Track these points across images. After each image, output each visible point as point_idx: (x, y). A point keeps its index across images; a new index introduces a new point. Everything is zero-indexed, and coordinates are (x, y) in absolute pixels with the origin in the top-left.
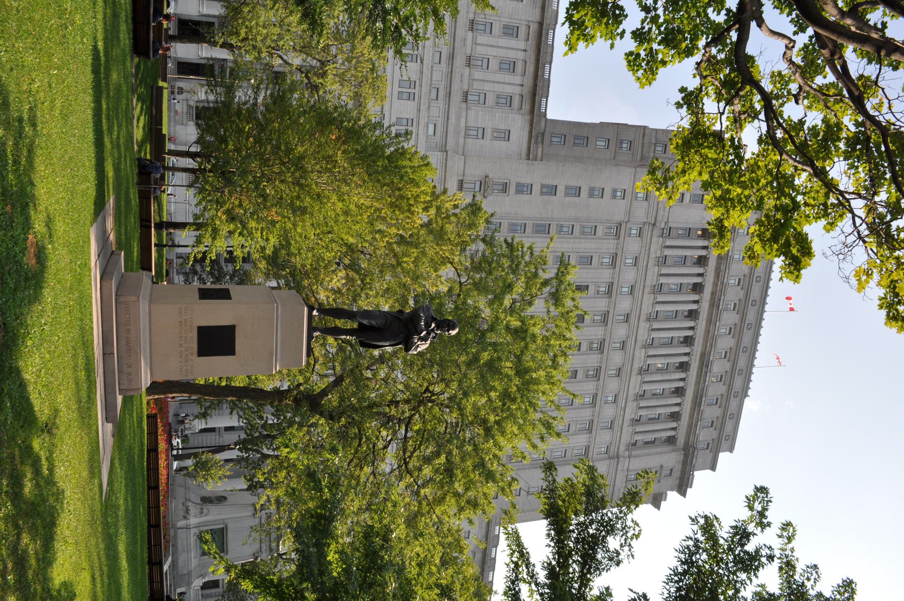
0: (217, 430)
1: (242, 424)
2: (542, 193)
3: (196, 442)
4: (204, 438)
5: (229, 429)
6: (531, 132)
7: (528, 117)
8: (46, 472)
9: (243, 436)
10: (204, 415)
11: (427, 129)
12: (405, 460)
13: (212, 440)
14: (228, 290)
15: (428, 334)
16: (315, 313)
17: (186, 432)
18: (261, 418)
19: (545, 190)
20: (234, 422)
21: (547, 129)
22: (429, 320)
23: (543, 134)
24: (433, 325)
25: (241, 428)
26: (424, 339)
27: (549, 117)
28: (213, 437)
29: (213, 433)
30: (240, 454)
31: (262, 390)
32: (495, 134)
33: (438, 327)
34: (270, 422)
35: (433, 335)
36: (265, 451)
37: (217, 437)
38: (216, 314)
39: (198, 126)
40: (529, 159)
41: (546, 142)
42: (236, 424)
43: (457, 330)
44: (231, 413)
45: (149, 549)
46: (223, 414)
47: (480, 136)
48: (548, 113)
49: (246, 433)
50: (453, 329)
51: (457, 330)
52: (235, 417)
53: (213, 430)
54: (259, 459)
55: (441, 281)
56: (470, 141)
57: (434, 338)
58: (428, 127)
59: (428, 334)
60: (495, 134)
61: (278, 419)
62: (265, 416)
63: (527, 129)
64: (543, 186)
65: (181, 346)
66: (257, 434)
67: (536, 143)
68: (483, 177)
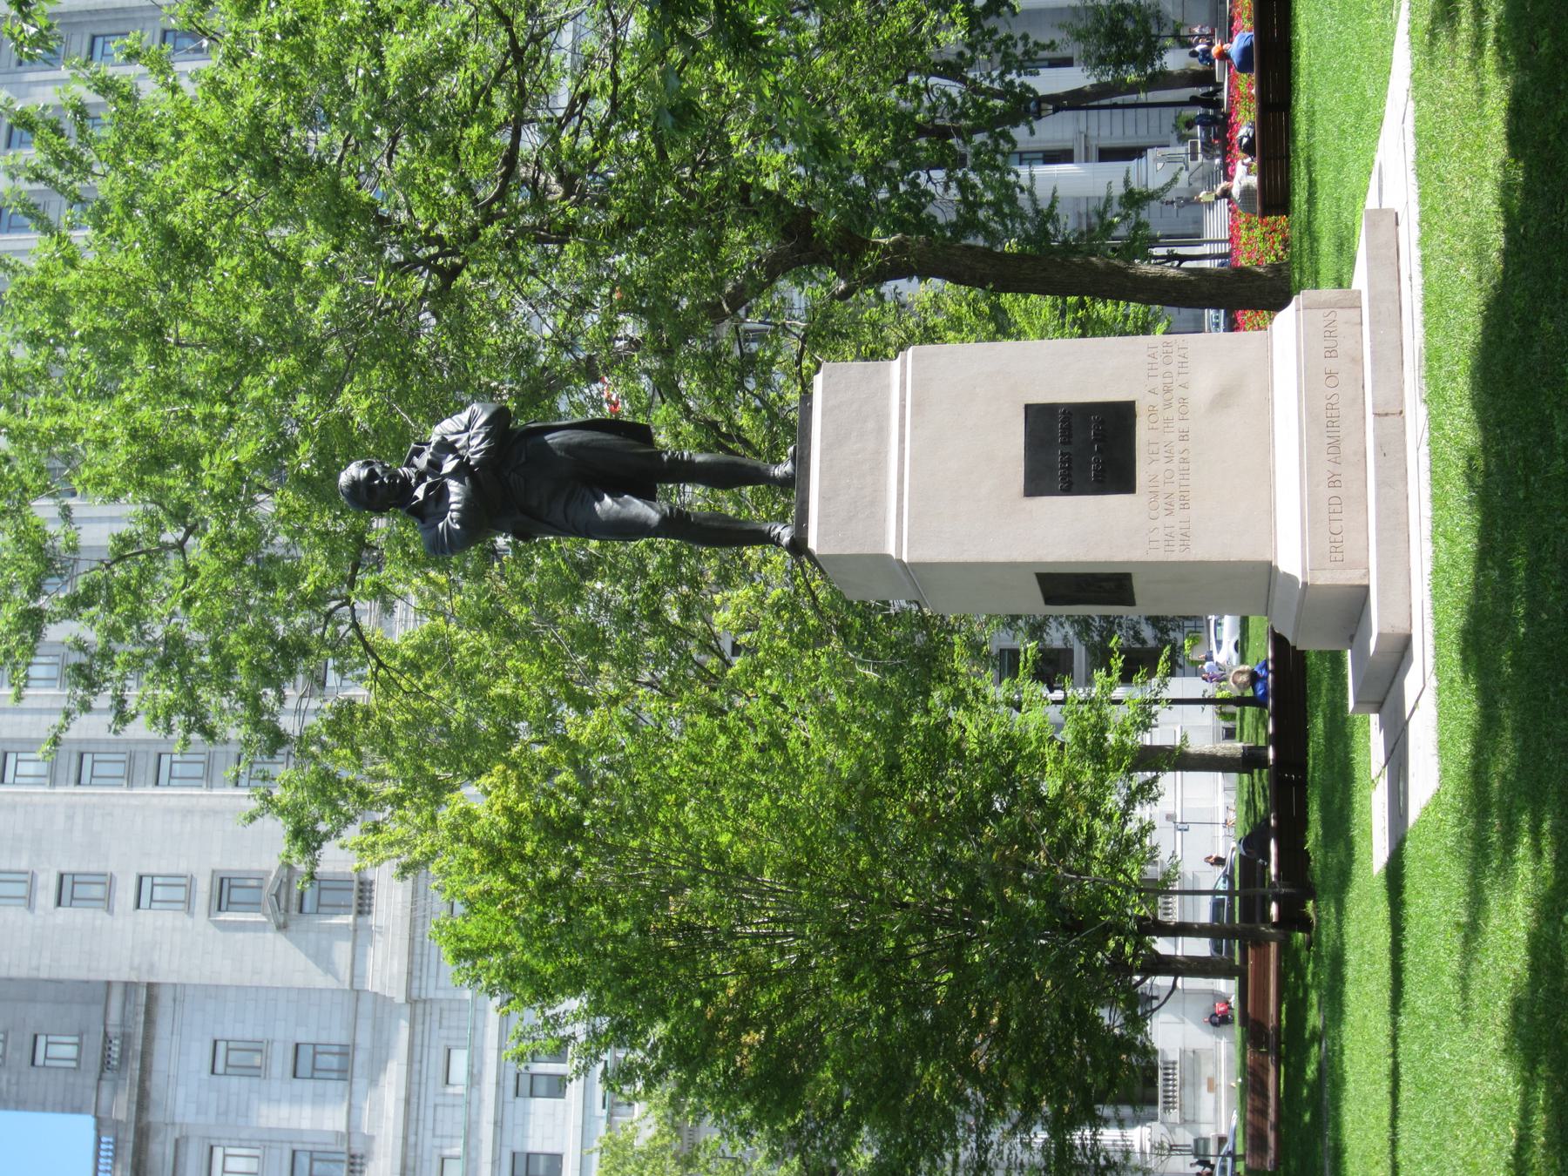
0: (1094, 154)
1: (1024, 171)
2: (108, 881)
3: (1154, 123)
4: (1130, 131)
5: (1052, 157)
6: (145, 1071)
7: (155, 1116)
8: (1284, 1007)
9: (1020, 133)
10: (1134, 199)
11: (471, 1066)
12: (518, 60)
13: (1109, 127)
14: (1049, 600)
15: (435, 465)
16: (786, 535)
17: (1181, 150)
18: (964, 186)
19: (97, 891)
20: (1048, 176)
21: (91, 1080)
22: (431, 508)
23: (105, 1064)
24: (420, 493)
25: (1026, 158)
26: (446, 447)
27: (87, 1122)
28: (1105, 132)
29: (1107, 143)
30: (1030, 81)
31: (957, 279)
32: (257, 1060)
33: (406, 487)
34: (939, 175)
35: (422, 462)
36: (954, 89)
37: (1093, 133)
38: (1081, 530)
39: (1148, 1052)
40: (150, 986)
41: (94, 1042)
42: (1041, 170)
43: (344, 479)
44: (1054, 199)
45: (411, 953)
46: (1077, 200)
47: (306, 1054)
48: (92, 1134)
49: (1013, 143)
50: (355, 484)
51: (344, 479)
52: (1043, 194)
53: (1106, 155)
54: (971, 63)
55: (405, 613)
56: (339, 1036)
57: (418, 453)
58: (471, 1074)
59: (435, 465)
60: (257, 1060)
61: (914, 184)
62: (954, 192)
63: (157, 1081)
64: (107, 902)
65: (1184, 437)
66: (978, 138)
67: (126, 1038)
68: (292, 927)
